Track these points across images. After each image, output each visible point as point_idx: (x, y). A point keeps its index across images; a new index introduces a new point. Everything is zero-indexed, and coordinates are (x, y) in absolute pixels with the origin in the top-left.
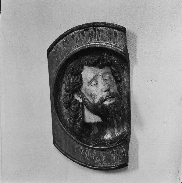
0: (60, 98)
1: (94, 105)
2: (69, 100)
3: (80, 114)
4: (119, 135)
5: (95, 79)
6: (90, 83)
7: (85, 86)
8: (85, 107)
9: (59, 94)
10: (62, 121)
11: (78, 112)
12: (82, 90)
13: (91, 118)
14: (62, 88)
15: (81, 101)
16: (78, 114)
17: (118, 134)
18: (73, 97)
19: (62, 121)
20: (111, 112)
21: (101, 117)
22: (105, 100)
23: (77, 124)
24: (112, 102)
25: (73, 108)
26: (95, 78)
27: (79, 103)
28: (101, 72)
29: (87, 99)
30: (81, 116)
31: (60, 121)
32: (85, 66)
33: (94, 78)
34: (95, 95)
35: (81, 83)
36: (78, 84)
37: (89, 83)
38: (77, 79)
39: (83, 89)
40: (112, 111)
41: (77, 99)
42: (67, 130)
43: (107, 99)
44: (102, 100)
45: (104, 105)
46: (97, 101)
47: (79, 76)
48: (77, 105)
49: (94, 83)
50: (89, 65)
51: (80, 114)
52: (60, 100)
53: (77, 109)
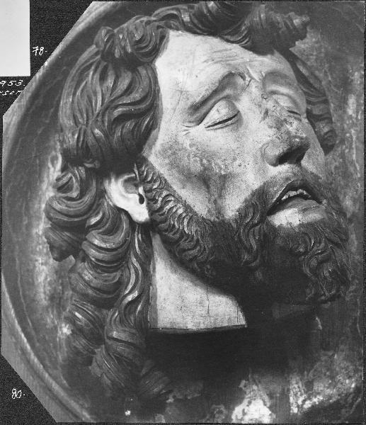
0: (29, 226)
1: (218, 229)
2: (76, 207)
3: (130, 287)
4: (308, 405)
5: (227, 98)
6: (198, 110)
7: (172, 126)
8: (157, 242)
9: (28, 209)
10: (33, 333)
11: (118, 274)
12: (156, 159)
13: (184, 303)
14: (42, 182)
15: (141, 213)
16: (120, 285)
17: (304, 401)
18: (102, 194)
19: (33, 333)
20: (316, 271)
21: (244, 304)
22: (280, 205)
23: (115, 334)
24: (314, 216)
25: (99, 248)
26: (228, 92)
27: (132, 222)
28: (259, 65)
29: (178, 200)
30: (136, 294)
31: (24, 330)
32: (172, 33)
33: (226, 86)
34: (225, 179)
35: (146, 111)
36: (140, 115)
37: (195, 108)
38: (128, 91)
39: (158, 146)
40: (321, 263)
41: (122, 204)
42: (55, 378)
43: (290, 199)
44: (263, 204)
45: (275, 231)
46: (233, 205)
47: (143, 72)
48: (120, 237)
49: (219, 111)
50: (192, 29)
51: (130, 287)
52: (29, 235)
53: (118, 260)
